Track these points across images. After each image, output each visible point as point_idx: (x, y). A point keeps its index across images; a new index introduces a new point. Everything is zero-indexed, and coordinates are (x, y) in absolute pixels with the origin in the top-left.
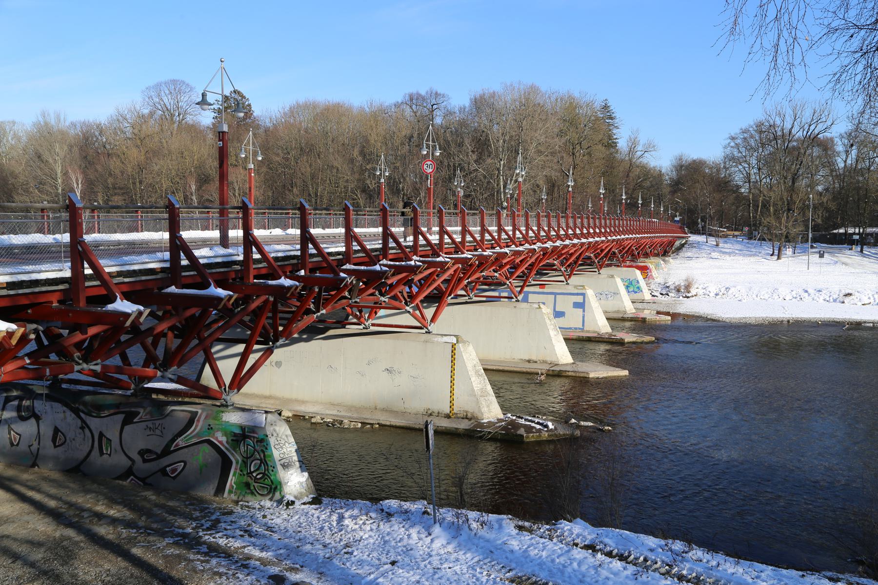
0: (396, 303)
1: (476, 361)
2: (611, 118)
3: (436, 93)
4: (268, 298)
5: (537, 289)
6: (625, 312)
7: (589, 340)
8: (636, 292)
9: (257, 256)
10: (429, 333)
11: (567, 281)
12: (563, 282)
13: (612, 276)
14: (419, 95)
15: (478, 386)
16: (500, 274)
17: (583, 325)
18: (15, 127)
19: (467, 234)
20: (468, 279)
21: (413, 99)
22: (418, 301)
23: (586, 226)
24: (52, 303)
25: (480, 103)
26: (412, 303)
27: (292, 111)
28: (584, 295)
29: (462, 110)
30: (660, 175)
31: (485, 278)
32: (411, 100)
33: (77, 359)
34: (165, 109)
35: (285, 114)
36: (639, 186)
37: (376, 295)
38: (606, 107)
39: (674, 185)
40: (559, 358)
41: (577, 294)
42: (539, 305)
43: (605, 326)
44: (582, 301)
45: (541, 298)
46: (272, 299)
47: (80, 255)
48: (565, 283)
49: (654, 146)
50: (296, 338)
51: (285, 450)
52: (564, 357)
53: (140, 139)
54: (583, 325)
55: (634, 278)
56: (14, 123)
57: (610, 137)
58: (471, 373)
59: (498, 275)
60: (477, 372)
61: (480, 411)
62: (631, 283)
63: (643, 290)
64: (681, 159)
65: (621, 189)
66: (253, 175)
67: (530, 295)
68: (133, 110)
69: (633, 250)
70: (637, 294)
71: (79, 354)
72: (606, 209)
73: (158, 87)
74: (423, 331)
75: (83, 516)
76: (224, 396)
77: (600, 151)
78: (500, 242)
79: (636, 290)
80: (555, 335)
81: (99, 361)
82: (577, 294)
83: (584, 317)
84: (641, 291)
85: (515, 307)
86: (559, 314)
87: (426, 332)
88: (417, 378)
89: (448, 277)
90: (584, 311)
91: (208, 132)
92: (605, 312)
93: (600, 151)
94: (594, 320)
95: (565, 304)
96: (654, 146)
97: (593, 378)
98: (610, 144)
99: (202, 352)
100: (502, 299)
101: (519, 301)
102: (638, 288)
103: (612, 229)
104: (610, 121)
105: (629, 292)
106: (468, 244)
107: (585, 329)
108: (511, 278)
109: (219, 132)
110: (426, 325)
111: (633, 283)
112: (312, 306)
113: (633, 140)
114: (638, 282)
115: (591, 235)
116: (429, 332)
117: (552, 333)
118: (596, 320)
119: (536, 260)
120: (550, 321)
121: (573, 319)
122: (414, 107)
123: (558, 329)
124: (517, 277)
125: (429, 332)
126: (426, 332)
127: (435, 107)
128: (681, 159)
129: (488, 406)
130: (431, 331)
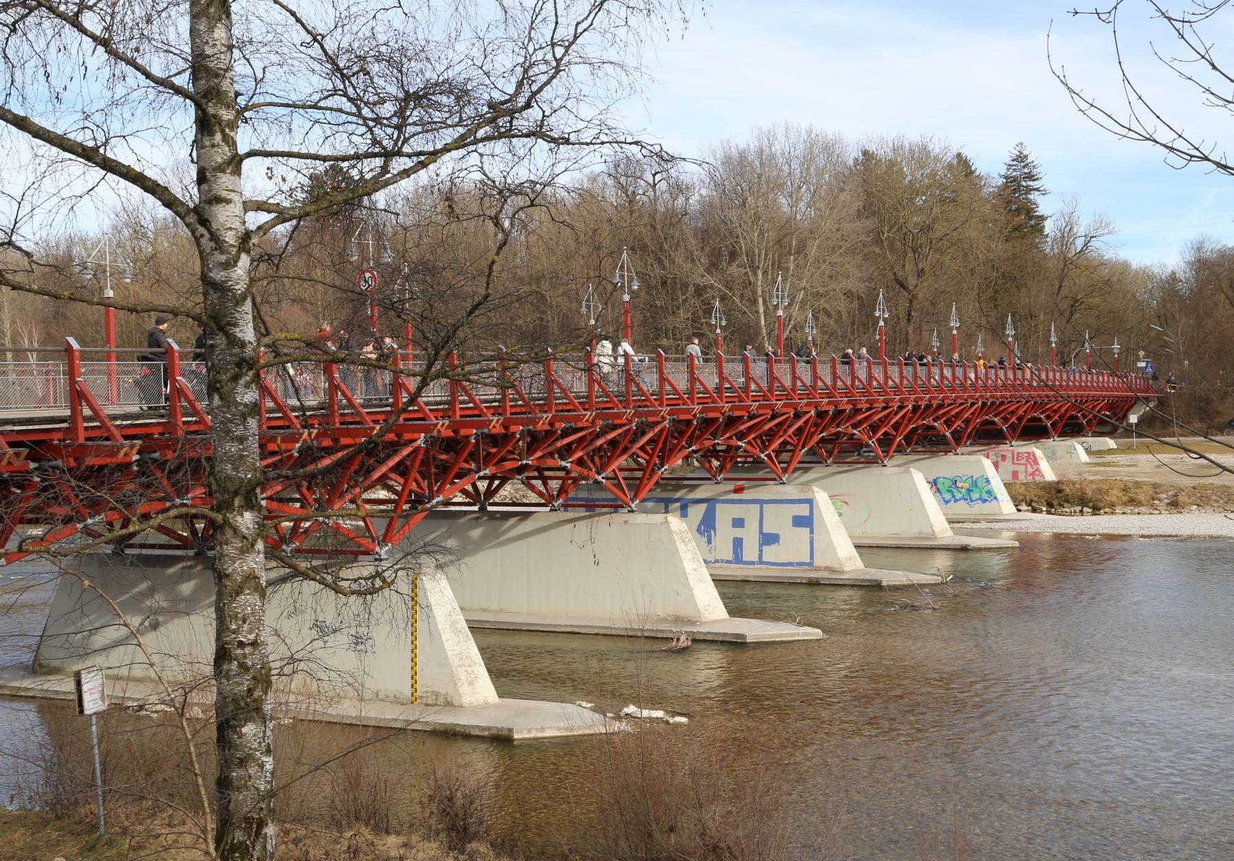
2: (1030, 177)
6: (934, 536)
7: (814, 584)
8: (986, 501)
9: (87, 412)
15: (455, 648)
17: (812, 557)
28: (810, 502)
40: (702, 610)
43: (850, 559)
44: (807, 513)
52: (710, 609)
54: (812, 557)
57: (1028, 210)
60: (453, 624)
62: (975, 484)
63: (999, 497)
64: (1199, 249)
65: (949, 307)
72: (1053, 339)
79: (985, 496)
80: (695, 570)
83: (812, 543)
84: (996, 498)
85: (626, 522)
90: (812, 532)
94: (831, 546)
101: (633, 511)
102: (989, 492)
104: (1031, 183)
105: (972, 501)
111: (979, 484)
114: (988, 481)
117: (689, 566)
118: (835, 548)
120: (686, 545)
127: (658, 177)
129: (471, 683)
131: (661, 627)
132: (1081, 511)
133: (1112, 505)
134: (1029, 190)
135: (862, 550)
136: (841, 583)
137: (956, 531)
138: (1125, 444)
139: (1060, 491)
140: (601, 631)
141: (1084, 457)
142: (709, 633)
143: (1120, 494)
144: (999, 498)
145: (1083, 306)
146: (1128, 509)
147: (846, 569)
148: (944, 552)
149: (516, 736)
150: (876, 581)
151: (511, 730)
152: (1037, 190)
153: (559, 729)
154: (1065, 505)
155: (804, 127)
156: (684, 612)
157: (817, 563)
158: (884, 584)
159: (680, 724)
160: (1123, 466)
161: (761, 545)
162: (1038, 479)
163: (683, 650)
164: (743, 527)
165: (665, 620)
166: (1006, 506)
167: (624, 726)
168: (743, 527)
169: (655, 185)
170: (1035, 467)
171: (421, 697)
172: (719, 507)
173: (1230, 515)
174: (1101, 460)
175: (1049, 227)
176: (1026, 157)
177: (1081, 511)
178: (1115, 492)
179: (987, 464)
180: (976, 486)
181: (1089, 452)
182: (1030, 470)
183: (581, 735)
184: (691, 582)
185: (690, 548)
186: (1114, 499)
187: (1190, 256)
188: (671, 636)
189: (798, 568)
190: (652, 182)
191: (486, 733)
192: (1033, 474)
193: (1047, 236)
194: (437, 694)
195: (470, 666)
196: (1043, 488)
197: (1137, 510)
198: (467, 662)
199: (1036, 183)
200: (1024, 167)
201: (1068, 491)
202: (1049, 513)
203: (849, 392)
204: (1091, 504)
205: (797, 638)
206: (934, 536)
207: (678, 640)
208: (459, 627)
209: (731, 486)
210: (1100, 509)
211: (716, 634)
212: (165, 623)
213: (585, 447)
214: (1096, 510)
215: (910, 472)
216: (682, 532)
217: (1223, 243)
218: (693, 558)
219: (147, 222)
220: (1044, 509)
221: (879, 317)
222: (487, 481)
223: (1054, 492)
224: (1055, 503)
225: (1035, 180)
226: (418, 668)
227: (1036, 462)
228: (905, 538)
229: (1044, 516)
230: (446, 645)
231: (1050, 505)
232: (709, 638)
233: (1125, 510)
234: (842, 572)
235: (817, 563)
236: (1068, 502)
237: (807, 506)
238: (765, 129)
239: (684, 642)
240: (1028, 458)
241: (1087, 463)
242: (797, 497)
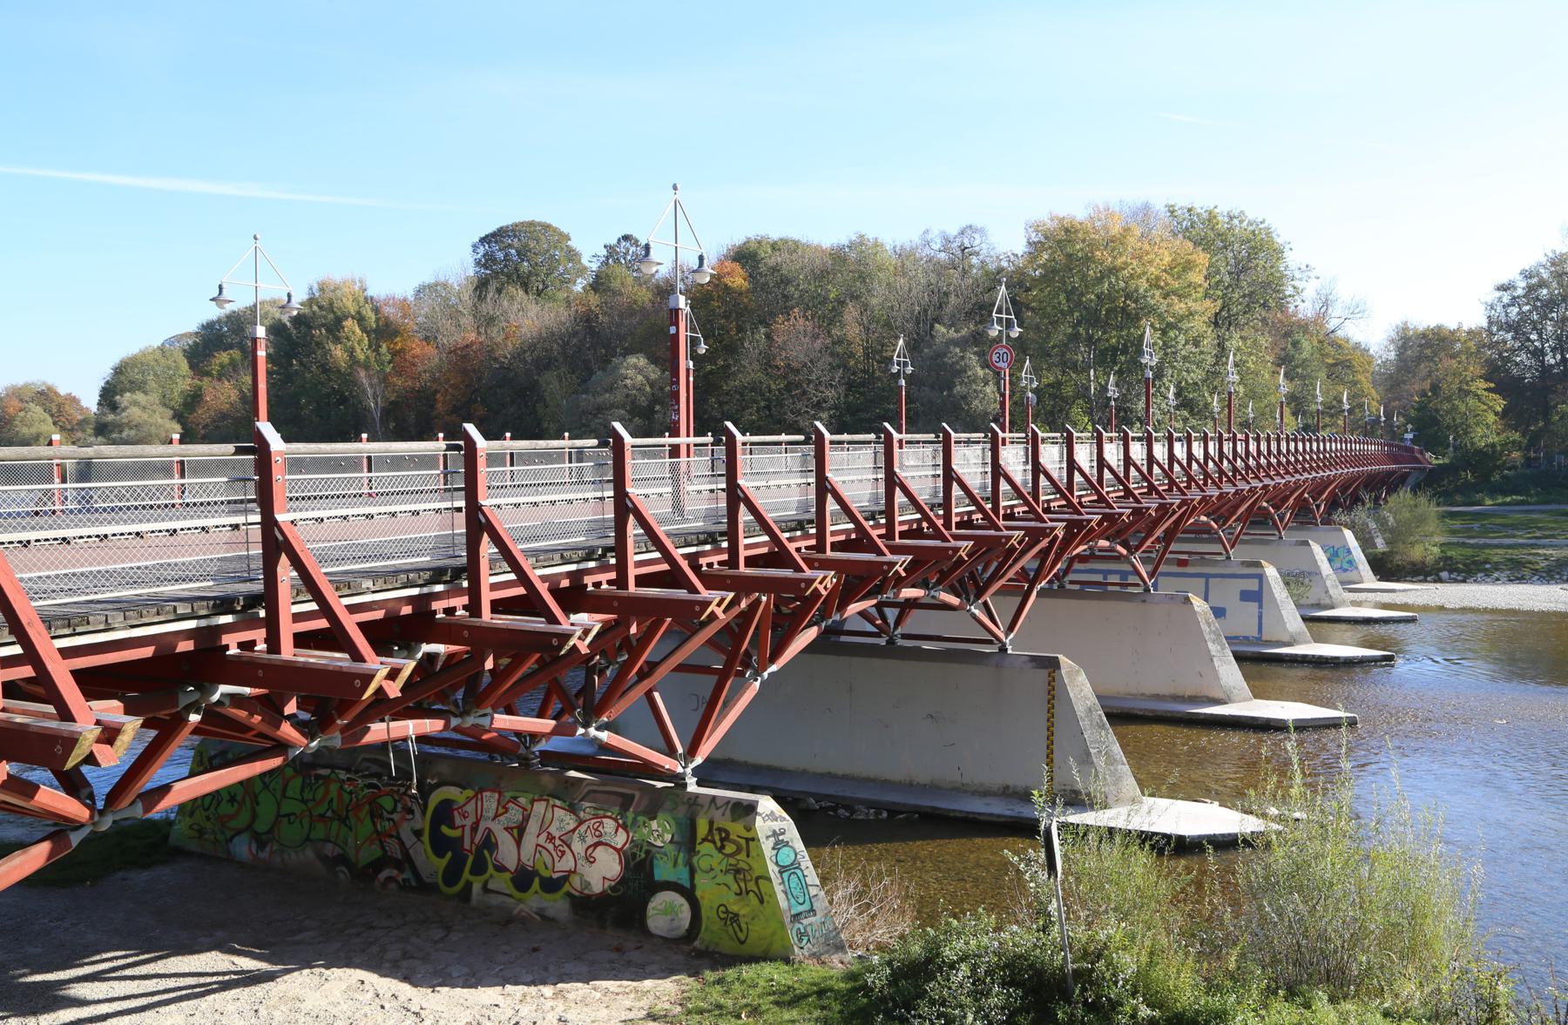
1: (1093, 700)
5: (1176, 569)
12: (1221, 554)
22: (987, 597)
44: (1256, 588)
48: (1223, 558)
50: (484, 661)
64: (1405, 329)
70: (1348, 573)
75: (450, 975)
79: (1346, 566)
83: (1260, 618)
84: (1357, 568)
102: (1350, 562)
107: (1264, 638)
114: (1349, 552)
117: (1213, 648)
118: (1285, 623)
121: (1243, 620)
123: (1224, 641)
128: (1405, 329)
164: (394, 681)
168: (394, 681)
173: (1565, 586)
180: (1338, 556)
191: (1151, 714)
203: (1094, 486)
213: (1089, 541)
219: (662, 1006)
221: (1026, 387)
222: (898, 610)
237: (1256, 581)
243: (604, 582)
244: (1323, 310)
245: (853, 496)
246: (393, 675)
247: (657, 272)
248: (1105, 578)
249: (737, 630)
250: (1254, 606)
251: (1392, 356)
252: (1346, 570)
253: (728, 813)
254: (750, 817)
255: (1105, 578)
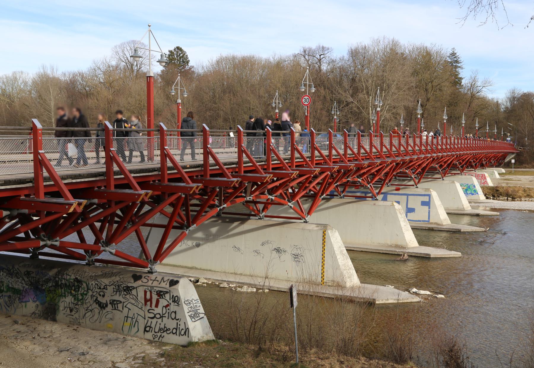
0: (282, 201)
2: (457, 62)
3: (323, 48)
4: (181, 195)
6: (464, 210)
7: (431, 230)
8: (473, 194)
10: (306, 222)
11: (416, 185)
13: (453, 182)
14: (310, 49)
16: (362, 180)
18: (24, 76)
19: (333, 149)
20: (336, 183)
21: (307, 53)
22: (297, 198)
23: (440, 144)
24: (150, 181)
25: (354, 54)
26: (293, 200)
27: (218, 62)
28: (429, 196)
29: (342, 59)
30: (497, 104)
31: (400, 173)
32: (305, 51)
33: (43, 237)
34: (127, 61)
35: (212, 65)
36: (476, 114)
37: (265, 194)
38: (453, 54)
39: (508, 113)
40: (408, 243)
41: (424, 195)
42: (393, 203)
44: (428, 200)
45: (397, 198)
46: (183, 196)
47: (40, 162)
49: (489, 82)
51: (192, 305)
52: (411, 242)
53: (109, 84)
55: (471, 184)
56: (22, 72)
57: (456, 75)
58: (337, 252)
59: (360, 180)
60: (341, 252)
61: (343, 280)
62: (469, 187)
63: (479, 193)
64: (513, 92)
66: (180, 107)
67: (388, 196)
68: (104, 61)
69: (470, 162)
71: (44, 233)
73: (116, 47)
74: (302, 221)
76: (150, 266)
77: (447, 90)
78: (371, 154)
79: (473, 192)
80: (405, 226)
81: (58, 238)
82: (424, 195)
83: (429, 213)
84: (477, 193)
85: (374, 204)
86: (410, 210)
87: (304, 222)
88: (297, 256)
89: (321, 180)
90: (429, 208)
91: (159, 77)
92: (411, 226)
93: (447, 90)
94: (437, 214)
95: (415, 202)
96: (489, 82)
97: (379, 304)
98: (457, 81)
99: (134, 233)
100: (367, 199)
102: (475, 191)
103: (459, 146)
104: (457, 64)
105: (467, 194)
106: (348, 156)
108: (371, 182)
109: (147, 77)
110: (304, 216)
112: (217, 202)
113: (473, 79)
114: (474, 186)
115: (444, 150)
116: (306, 222)
118: (439, 215)
119: (390, 169)
121: (421, 214)
122: (307, 57)
124: (376, 182)
125: (306, 222)
126: (304, 222)
127: (322, 56)
128: (513, 92)
130: (307, 221)
131: (393, 249)
132: (507, 199)
133: (520, 197)
134: (456, 67)
135: (450, 215)
136: (443, 229)
137: (473, 207)
138: (508, 171)
139: (497, 191)
140: (364, 250)
141: (498, 176)
142: (414, 253)
143: (523, 193)
144: (479, 193)
145: (479, 115)
146: (527, 199)
147: (444, 224)
148: (468, 216)
149: (377, 302)
150: (458, 229)
151: (374, 300)
152: (459, 67)
153: (395, 300)
154: (500, 196)
155: (391, 38)
156: (399, 243)
157: (431, 221)
158: (462, 231)
159: (442, 298)
160: (515, 180)
161: (407, 213)
162: (486, 185)
163: (406, 260)
165: (391, 246)
166: (482, 197)
167: (416, 299)
169: (320, 60)
170: (485, 180)
171: (326, 282)
172: (388, 196)
174: (504, 178)
175: (463, 82)
176: (456, 53)
177: (507, 199)
178: (521, 192)
179: (474, 179)
180: (470, 188)
181: (499, 174)
182: (483, 181)
183: (405, 303)
184: (404, 231)
185: (403, 216)
186: (521, 195)
187: (509, 95)
188: (401, 253)
189: (422, 223)
190: (319, 58)
192: (484, 183)
193: (463, 85)
194: (333, 281)
195: (349, 270)
196: (490, 189)
197: (530, 199)
198: (348, 268)
199: (459, 64)
200: (455, 58)
201: (501, 190)
202: (493, 199)
204: (511, 196)
205: (451, 256)
206: (464, 209)
207: (404, 255)
208: (344, 253)
209: (394, 188)
210: (515, 199)
211: (417, 253)
212: (203, 245)
214: (513, 199)
215: (454, 183)
216: (399, 209)
217: (522, 91)
218: (404, 220)
220: (492, 198)
223: (495, 191)
224: (496, 195)
225: (459, 63)
226: (325, 270)
227: (485, 178)
228: (454, 210)
229: (491, 201)
230: (339, 261)
231: (494, 196)
232: (413, 255)
233: (526, 199)
234: (442, 225)
235: (431, 221)
236: (501, 195)
237: (428, 197)
238: (376, 38)
239: (406, 257)
240: (482, 176)
241: (498, 179)
242: (423, 193)
243: (151, 181)
244: (473, 83)
245: (221, 158)
246: (80, 204)
247: (190, 120)
248: (366, 195)
249: (191, 193)
250: (426, 208)
251: (509, 104)
252: (473, 194)
253: (168, 284)
254: (177, 285)
255: (366, 195)
